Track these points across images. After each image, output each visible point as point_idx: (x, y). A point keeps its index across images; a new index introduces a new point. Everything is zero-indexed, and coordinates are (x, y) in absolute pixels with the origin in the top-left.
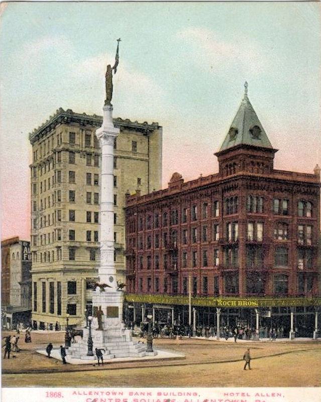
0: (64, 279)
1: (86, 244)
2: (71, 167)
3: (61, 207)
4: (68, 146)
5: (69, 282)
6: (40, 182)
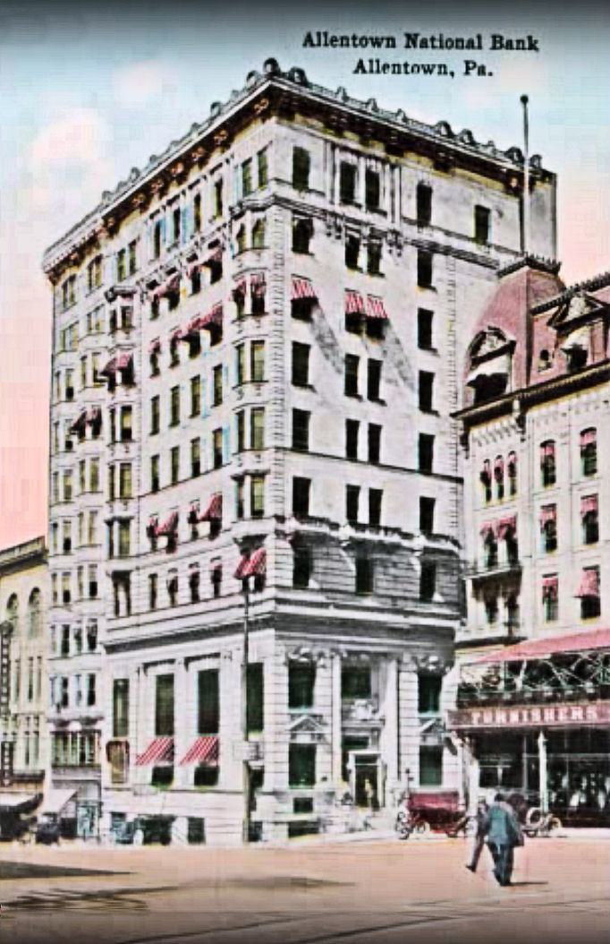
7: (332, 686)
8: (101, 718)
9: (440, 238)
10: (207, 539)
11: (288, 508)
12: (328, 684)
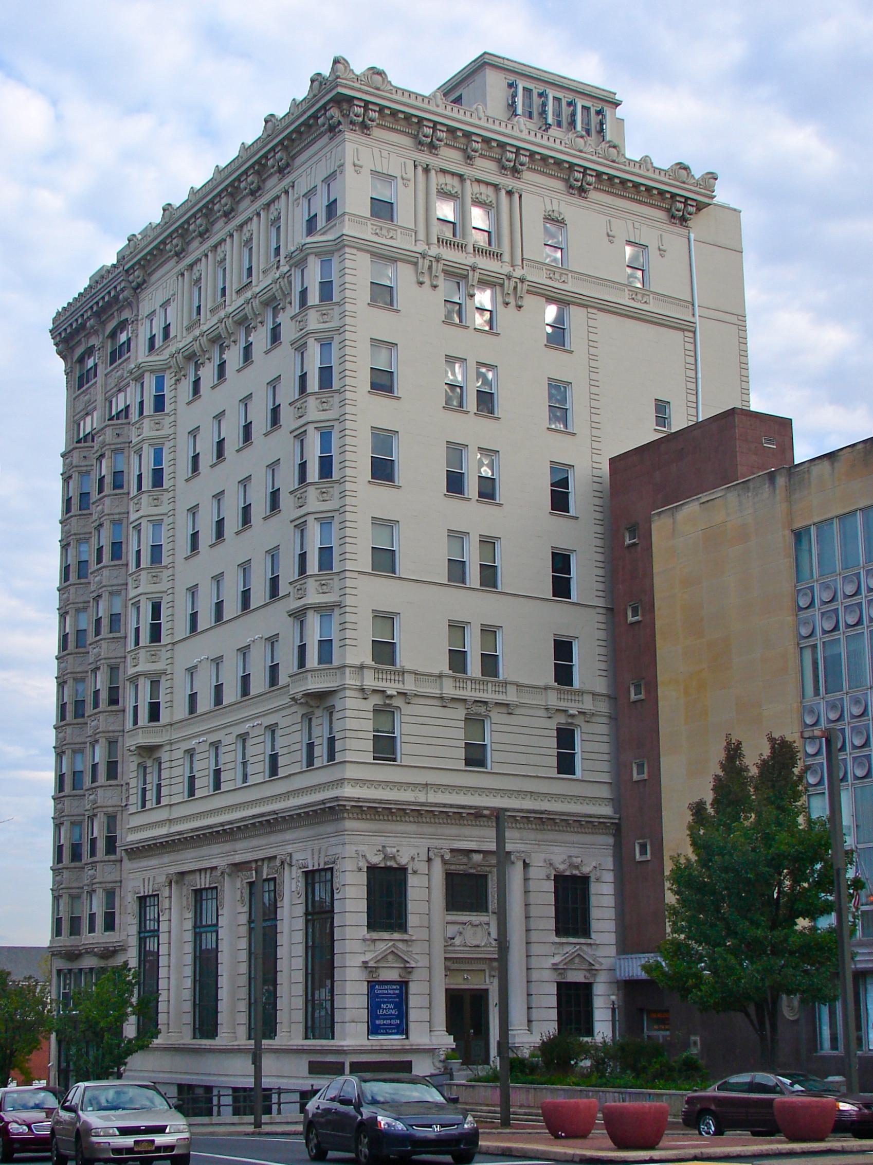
6: (183, 506)
12: (425, 894)
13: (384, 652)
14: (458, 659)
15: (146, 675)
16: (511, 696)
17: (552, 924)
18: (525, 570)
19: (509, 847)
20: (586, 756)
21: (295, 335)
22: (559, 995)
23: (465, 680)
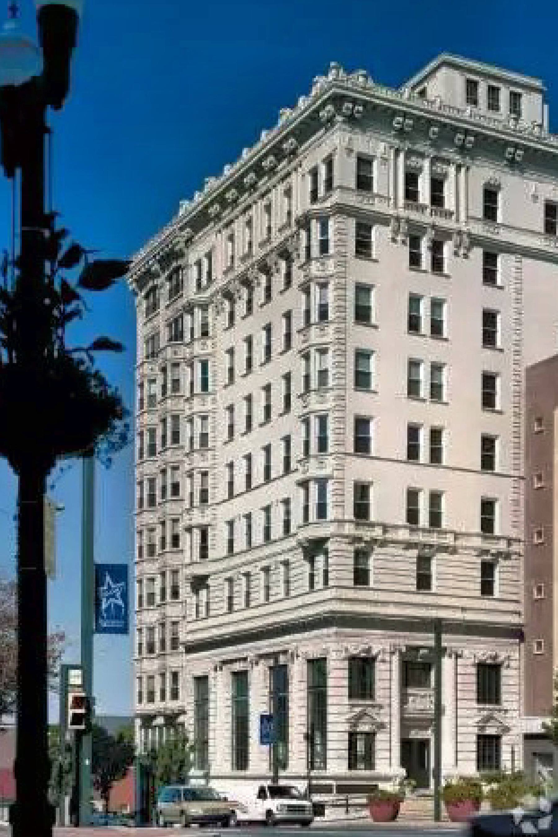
0: (336, 649)
1: (403, 535)
2: (361, 271)
3: (330, 405)
4: (353, 200)
5: (352, 659)
6: (222, 404)
7: (390, 671)
8: (184, 712)
9: (504, 236)
10: (323, 357)
11: (349, 514)
12: (387, 677)
13: (361, 511)
14: (412, 516)
15: (198, 526)
16: (449, 540)
17: (474, 696)
18: (460, 449)
19: (444, 644)
20: (502, 582)
21: (302, 279)
22: (478, 743)
23: (418, 529)
